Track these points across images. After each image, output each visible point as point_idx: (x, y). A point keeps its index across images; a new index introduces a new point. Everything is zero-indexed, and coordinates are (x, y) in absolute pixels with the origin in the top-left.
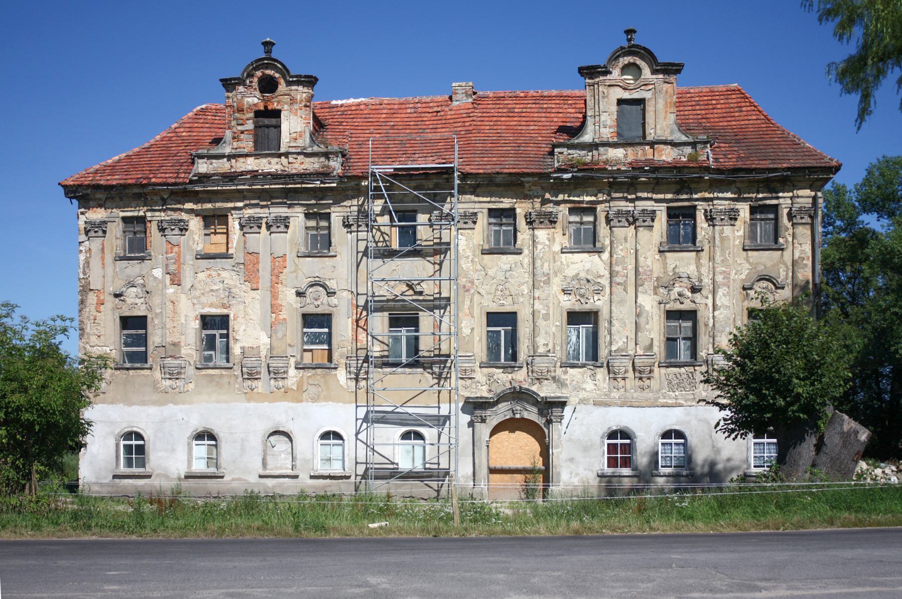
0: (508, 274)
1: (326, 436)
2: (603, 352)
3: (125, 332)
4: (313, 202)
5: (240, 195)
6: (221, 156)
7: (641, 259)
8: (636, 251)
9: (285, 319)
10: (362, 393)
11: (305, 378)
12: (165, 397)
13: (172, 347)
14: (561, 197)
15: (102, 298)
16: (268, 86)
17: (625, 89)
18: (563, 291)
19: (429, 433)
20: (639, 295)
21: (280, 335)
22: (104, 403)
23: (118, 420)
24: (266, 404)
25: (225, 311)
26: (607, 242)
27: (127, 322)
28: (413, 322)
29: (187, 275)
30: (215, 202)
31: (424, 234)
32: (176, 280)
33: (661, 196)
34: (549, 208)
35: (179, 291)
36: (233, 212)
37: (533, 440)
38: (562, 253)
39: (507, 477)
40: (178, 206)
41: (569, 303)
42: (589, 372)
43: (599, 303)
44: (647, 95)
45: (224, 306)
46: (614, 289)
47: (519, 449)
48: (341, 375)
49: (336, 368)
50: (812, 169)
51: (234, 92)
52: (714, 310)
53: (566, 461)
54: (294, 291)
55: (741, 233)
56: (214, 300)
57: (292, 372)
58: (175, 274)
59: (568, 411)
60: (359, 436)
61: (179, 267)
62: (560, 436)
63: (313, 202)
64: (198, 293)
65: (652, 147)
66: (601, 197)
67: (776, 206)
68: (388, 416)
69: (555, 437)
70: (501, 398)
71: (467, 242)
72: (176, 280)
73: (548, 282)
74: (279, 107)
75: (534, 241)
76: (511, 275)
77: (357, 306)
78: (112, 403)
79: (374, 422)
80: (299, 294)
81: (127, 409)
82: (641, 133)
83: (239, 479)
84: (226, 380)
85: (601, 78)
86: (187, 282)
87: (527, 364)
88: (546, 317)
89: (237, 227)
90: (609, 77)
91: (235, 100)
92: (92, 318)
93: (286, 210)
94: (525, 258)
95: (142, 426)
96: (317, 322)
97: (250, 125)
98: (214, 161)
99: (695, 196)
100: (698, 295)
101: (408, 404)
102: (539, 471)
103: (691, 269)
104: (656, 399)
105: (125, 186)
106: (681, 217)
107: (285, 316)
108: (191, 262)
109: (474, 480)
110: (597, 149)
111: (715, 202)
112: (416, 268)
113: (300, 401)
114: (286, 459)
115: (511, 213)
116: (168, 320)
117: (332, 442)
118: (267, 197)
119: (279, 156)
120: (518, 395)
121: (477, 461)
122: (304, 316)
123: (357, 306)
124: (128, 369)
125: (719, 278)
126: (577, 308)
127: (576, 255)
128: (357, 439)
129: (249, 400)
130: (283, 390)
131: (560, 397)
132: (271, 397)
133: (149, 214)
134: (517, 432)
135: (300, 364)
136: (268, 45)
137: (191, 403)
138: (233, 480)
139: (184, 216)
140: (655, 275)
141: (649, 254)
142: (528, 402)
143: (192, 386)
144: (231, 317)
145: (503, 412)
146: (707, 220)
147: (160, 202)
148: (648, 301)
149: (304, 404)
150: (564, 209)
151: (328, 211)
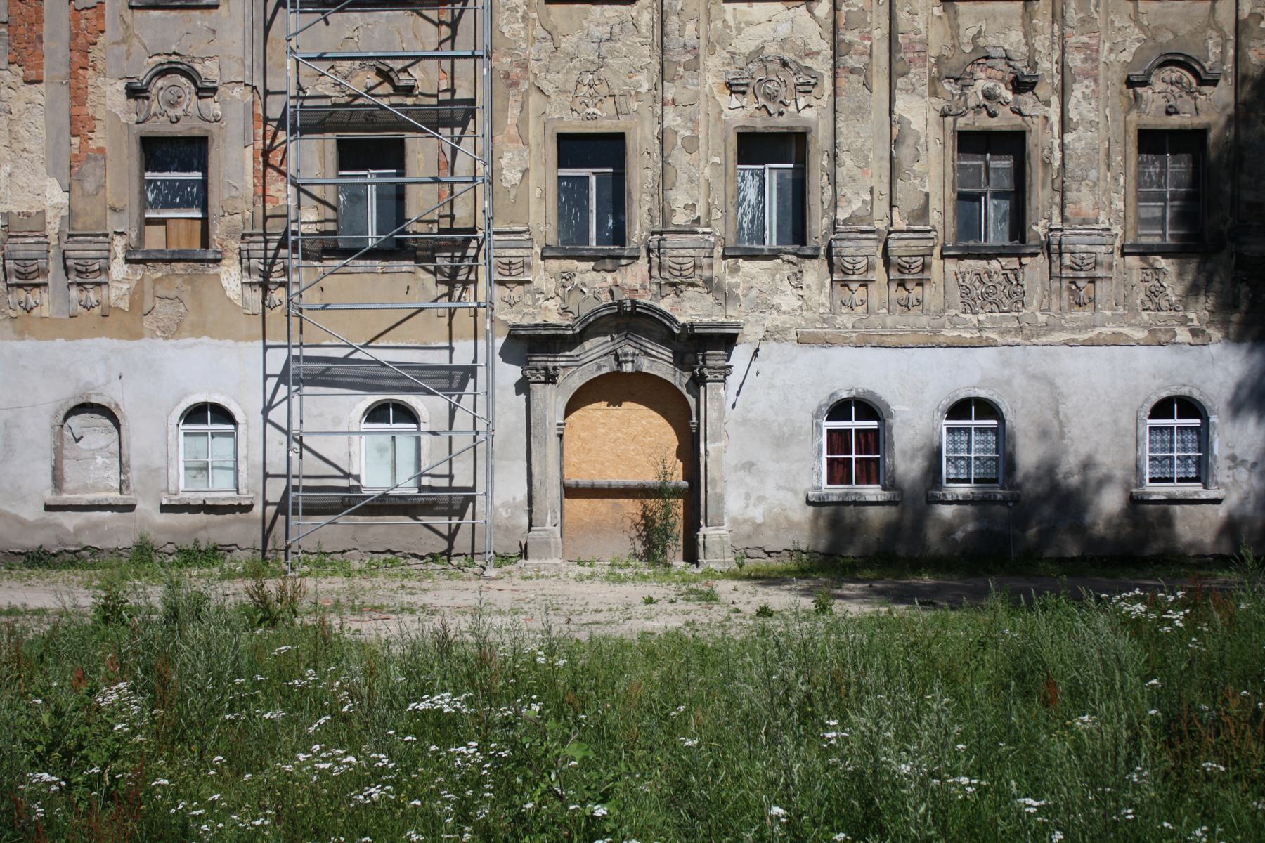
0: (605, 48)
2: (818, 225)
11: (148, 285)
18: (729, 85)
19: (427, 406)
24: (60, 342)
37: (662, 421)
39: (602, 506)
41: (741, 113)
42: (787, 270)
43: (808, 113)
46: (841, 82)
47: (630, 442)
48: (230, 277)
49: (217, 261)
52: (1063, 131)
53: (736, 468)
54: (121, 85)
57: (119, 269)
59: (740, 356)
60: (272, 415)
62: (721, 411)
69: (712, 415)
70: (592, 327)
73: (694, 66)
76: (611, 51)
77: (266, 120)
80: (135, 92)
87: (649, 251)
88: (691, 145)
100: (1027, 98)
102: (677, 492)
103: (1013, 40)
104: (937, 330)
107: (101, 143)
109: (530, 512)
113: (136, 335)
120: (629, 320)
123: (266, 120)
126: (760, 123)
128: (266, 421)
130: (97, 311)
131: (722, 325)
132: (73, 326)
134: (626, 405)
140: (933, 52)
142: (651, 338)
145: (594, 358)
148: (917, 111)
149: (145, 342)
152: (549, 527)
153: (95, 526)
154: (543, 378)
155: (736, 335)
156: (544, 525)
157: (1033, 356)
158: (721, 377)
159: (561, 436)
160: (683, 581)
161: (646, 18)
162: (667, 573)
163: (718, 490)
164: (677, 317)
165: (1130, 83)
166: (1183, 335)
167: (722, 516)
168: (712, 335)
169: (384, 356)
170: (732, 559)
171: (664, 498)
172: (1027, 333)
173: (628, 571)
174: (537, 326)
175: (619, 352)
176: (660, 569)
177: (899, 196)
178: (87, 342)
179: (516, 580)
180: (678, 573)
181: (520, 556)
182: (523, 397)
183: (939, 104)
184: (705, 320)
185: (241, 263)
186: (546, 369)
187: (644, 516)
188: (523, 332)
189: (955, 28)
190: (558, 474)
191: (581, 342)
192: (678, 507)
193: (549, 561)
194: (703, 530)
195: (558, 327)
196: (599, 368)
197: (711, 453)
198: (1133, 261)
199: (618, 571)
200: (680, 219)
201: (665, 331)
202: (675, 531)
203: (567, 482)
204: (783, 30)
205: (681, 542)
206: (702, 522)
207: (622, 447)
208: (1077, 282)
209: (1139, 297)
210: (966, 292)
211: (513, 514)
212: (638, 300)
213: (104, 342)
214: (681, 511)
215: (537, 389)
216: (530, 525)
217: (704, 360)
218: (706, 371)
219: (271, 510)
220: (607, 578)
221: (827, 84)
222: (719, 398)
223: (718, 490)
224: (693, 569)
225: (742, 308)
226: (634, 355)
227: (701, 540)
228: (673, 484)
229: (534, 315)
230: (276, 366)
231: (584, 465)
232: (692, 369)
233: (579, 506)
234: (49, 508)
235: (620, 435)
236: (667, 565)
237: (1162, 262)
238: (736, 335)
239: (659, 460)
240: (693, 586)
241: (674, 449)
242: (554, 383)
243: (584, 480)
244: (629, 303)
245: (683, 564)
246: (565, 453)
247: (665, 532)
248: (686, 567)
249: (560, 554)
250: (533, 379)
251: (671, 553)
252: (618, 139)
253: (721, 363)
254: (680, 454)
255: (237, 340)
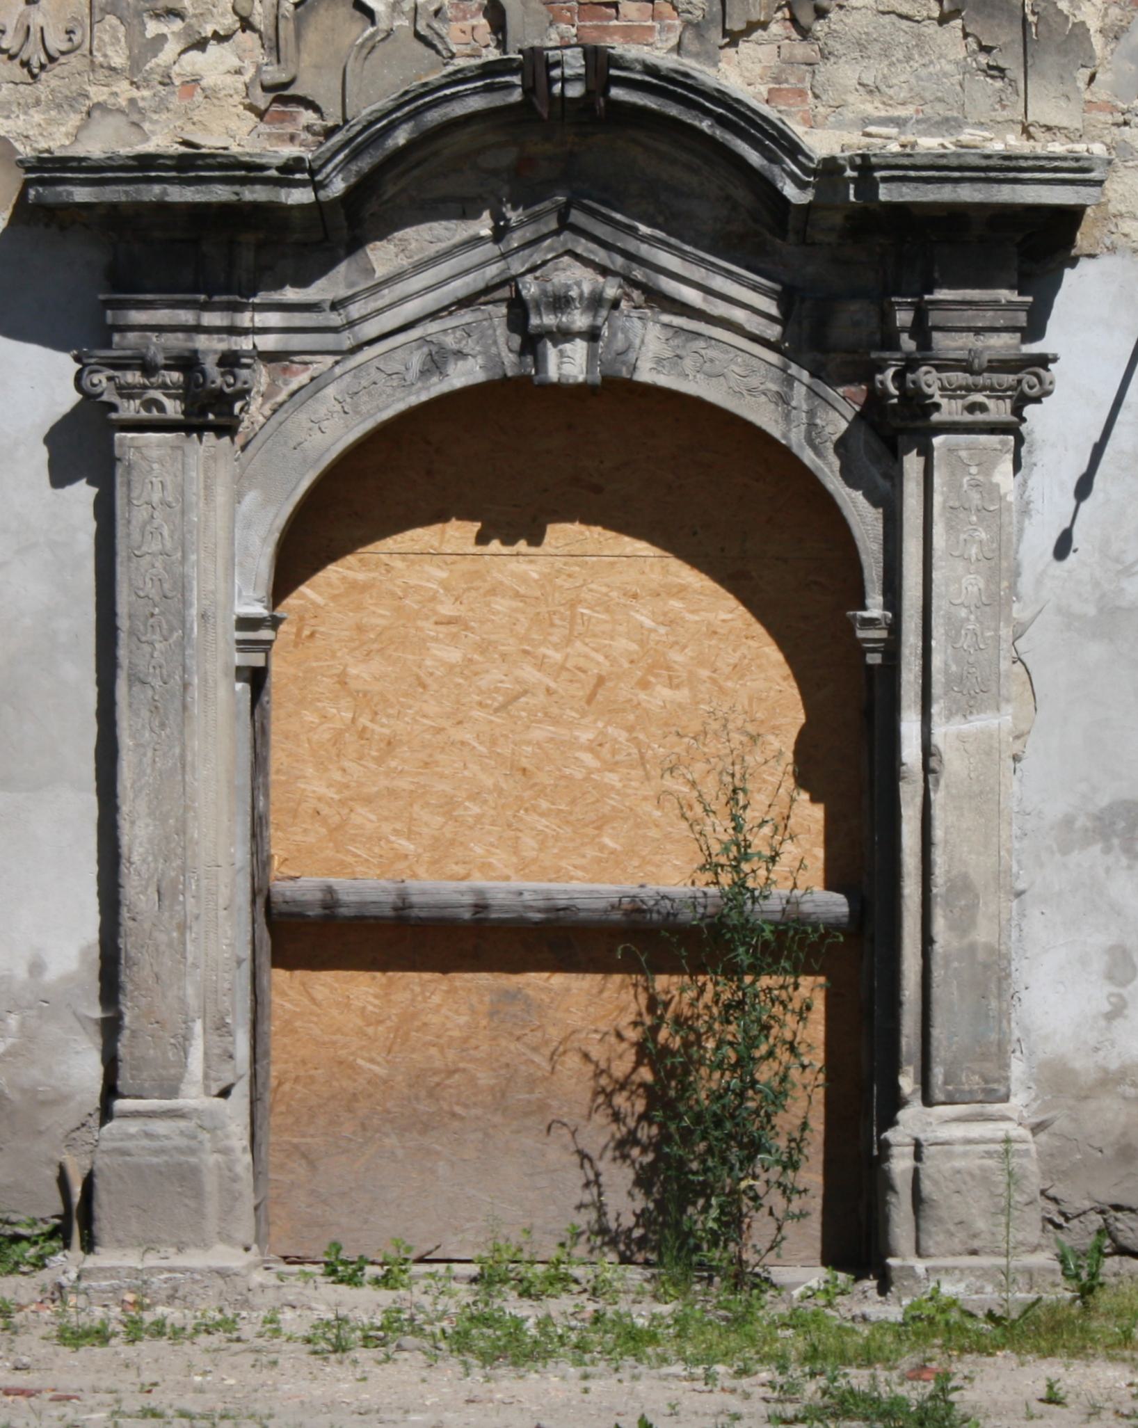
37: (727, 611)
39: (447, 1004)
40: (604, 210)
47: (574, 709)
53: (1069, 834)
59: (1089, 321)
62: (1002, 570)
69: (958, 584)
70: (402, 174)
102: (792, 943)
109: (111, 1029)
121: (136, 835)
131: (1007, 168)
134: (563, 535)
142: (679, 227)
145: (409, 317)
152: (199, 1104)
154: (173, 409)
155: (1070, 217)
156: (172, 1091)
158: (1000, 411)
159: (257, 679)
160: (813, 1355)
162: (739, 1321)
163: (983, 934)
164: (797, 129)
167: (1000, 1054)
168: (957, 214)
170: (1044, 1259)
171: (733, 971)
173: (561, 1306)
174: (146, 162)
175: (530, 288)
176: (709, 1300)
179: (32, 1346)
180: (795, 1321)
181: (60, 1233)
182: (83, 493)
184: (929, 143)
186: (188, 363)
187: (646, 1051)
188: (82, 194)
190: (241, 853)
191: (355, 245)
192: (801, 1014)
193: (195, 1259)
194: (913, 1120)
195: (249, 171)
196: (437, 362)
197: (953, 763)
199: (513, 1305)
201: (741, 194)
202: (786, 1121)
203: (282, 888)
205: (812, 1176)
206: (907, 1083)
207: (540, 733)
211: (28, 1036)
212: (620, 47)
214: (815, 1031)
215: (146, 453)
216: (110, 1091)
217: (921, 331)
218: (929, 380)
220: (461, 1342)
222: (991, 510)
223: (983, 934)
224: (866, 1304)
225: (1101, 92)
226: (595, 302)
227: (900, 1165)
228: (774, 905)
229: (135, 115)
231: (363, 816)
232: (865, 372)
233: (337, 1004)
235: (529, 673)
236: (744, 1280)
238: (1070, 217)
239: (710, 788)
240: (858, 1378)
241: (784, 742)
242: (227, 428)
243: (365, 883)
244: (574, 63)
245: (817, 1276)
246: (278, 757)
247: (738, 1133)
248: (830, 1293)
249: (245, 1229)
250: (130, 409)
251: (760, 1229)
253: (1002, 344)
254: (810, 768)
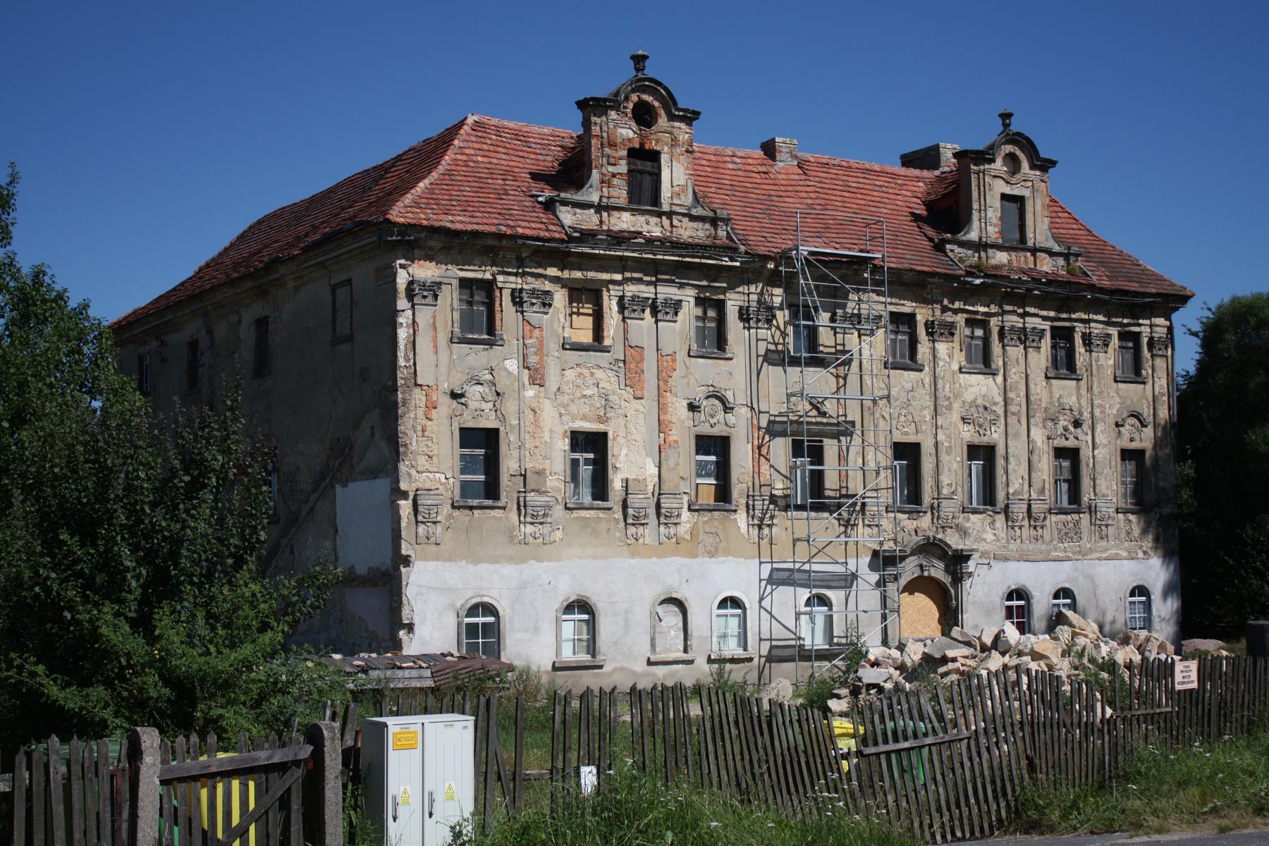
0: (911, 394)
1: (723, 603)
2: (1000, 496)
3: (467, 451)
4: (705, 283)
5: (622, 265)
6: (585, 206)
7: (1032, 386)
8: (1027, 376)
9: (676, 442)
10: (765, 542)
11: (700, 524)
12: (524, 550)
13: (536, 477)
14: (957, 305)
15: (435, 398)
16: (644, 116)
17: (1007, 182)
18: (963, 419)
19: (835, 596)
20: (1032, 428)
21: (672, 463)
22: (437, 560)
23: (460, 586)
24: (654, 559)
25: (600, 427)
26: (1001, 363)
27: (469, 437)
28: (817, 455)
29: (552, 372)
30: (587, 270)
31: (826, 338)
32: (537, 378)
33: (1044, 313)
34: (949, 317)
35: (542, 395)
36: (611, 287)
38: (961, 372)
41: (968, 434)
42: (989, 520)
43: (995, 436)
44: (1026, 193)
45: (600, 420)
46: (1009, 420)
48: (741, 518)
49: (735, 511)
50: (1166, 296)
51: (604, 118)
52: (1094, 449)
54: (685, 403)
55: (1111, 362)
56: (586, 410)
57: (686, 515)
58: (536, 370)
60: (763, 604)
61: (541, 359)
63: (705, 283)
64: (566, 399)
65: (1034, 255)
66: (994, 309)
67: (1139, 333)
68: (797, 576)
71: (872, 348)
72: (537, 378)
73: (949, 408)
74: (658, 148)
75: (934, 356)
76: (913, 397)
77: (759, 428)
78: (450, 560)
79: (778, 585)
80: (693, 407)
81: (471, 568)
82: (1017, 236)
83: (622, 669)
84: (603, 526)
85: (987, 166)
86: (552, 382)
87: (932, 508)
88: (949, 451)
89: (615, 308)
90: (993, 166)
91: (605, 128)
92: (419, 428)
93: (675, 290)
94: (926, 376)
95: (495, 594)
96: (715, 447)
97: (623, 168)
98: (578, 211)
99: (1074, 316)
100: (1079, 430)
101: (814, 560)
103: (1072, 401)
104: (1049, 552)
105: (475, 234)
106: (480, 295)
107: (675, 438)
108: (556, 354)
110: (985, 251)
111: (1092, 325)
112: (818, 381)
113: (695, 556)
114: (676, 637)
115: (488, 287)
116: (527, 436)
117: (730, 611)
118: (655, 270)
119: (660, 215)
120: (931, 548)
122: (463, 431)
123: (759, 428)
124: (471, 508)
125: (1097, 412)
126: (977, 440)
127: (973, 376)
128: (761, 607)
129: (633, 555)
130: (674, 540)
132: (660, 549)
133: (500, 278)
135: (695, 504)
136: (639, 60)
137: (559, 559)
138: (615, 670)
139: (548, 286)
140: (1044, 405)
141: (1038, 380)
143: (559, 534)
144: (610, 436)
145: (909, 569)
146: (1085, 344)
147: (514, 262)
148: (1038, 435)
149: (699, 560)
150: (960, 319)
151: (722, 297)
153: (673, 674)
157: (1084, 565)
161: (927, 380)
165: (1117, 425)
166: (1141, 555)
169: (815, 567)
172: (1083, 554)
177: (1033, 480)
178: (669, 559)
183: (1046, 432)
185: (748, 512)
189: (1051, 393)
198: (1121, 516)
200: (945, 491)
204: (984, 390)
208: (1099, 525)
209: (1123, 535)
210: (1059, 531)
213: (678, 560)
219: (763, 660)
221: (1002, 419)
230: (765, 575)
234: (650, 663)
237: (1131, 517)
252: (916, 447)
255: (746, 558)
